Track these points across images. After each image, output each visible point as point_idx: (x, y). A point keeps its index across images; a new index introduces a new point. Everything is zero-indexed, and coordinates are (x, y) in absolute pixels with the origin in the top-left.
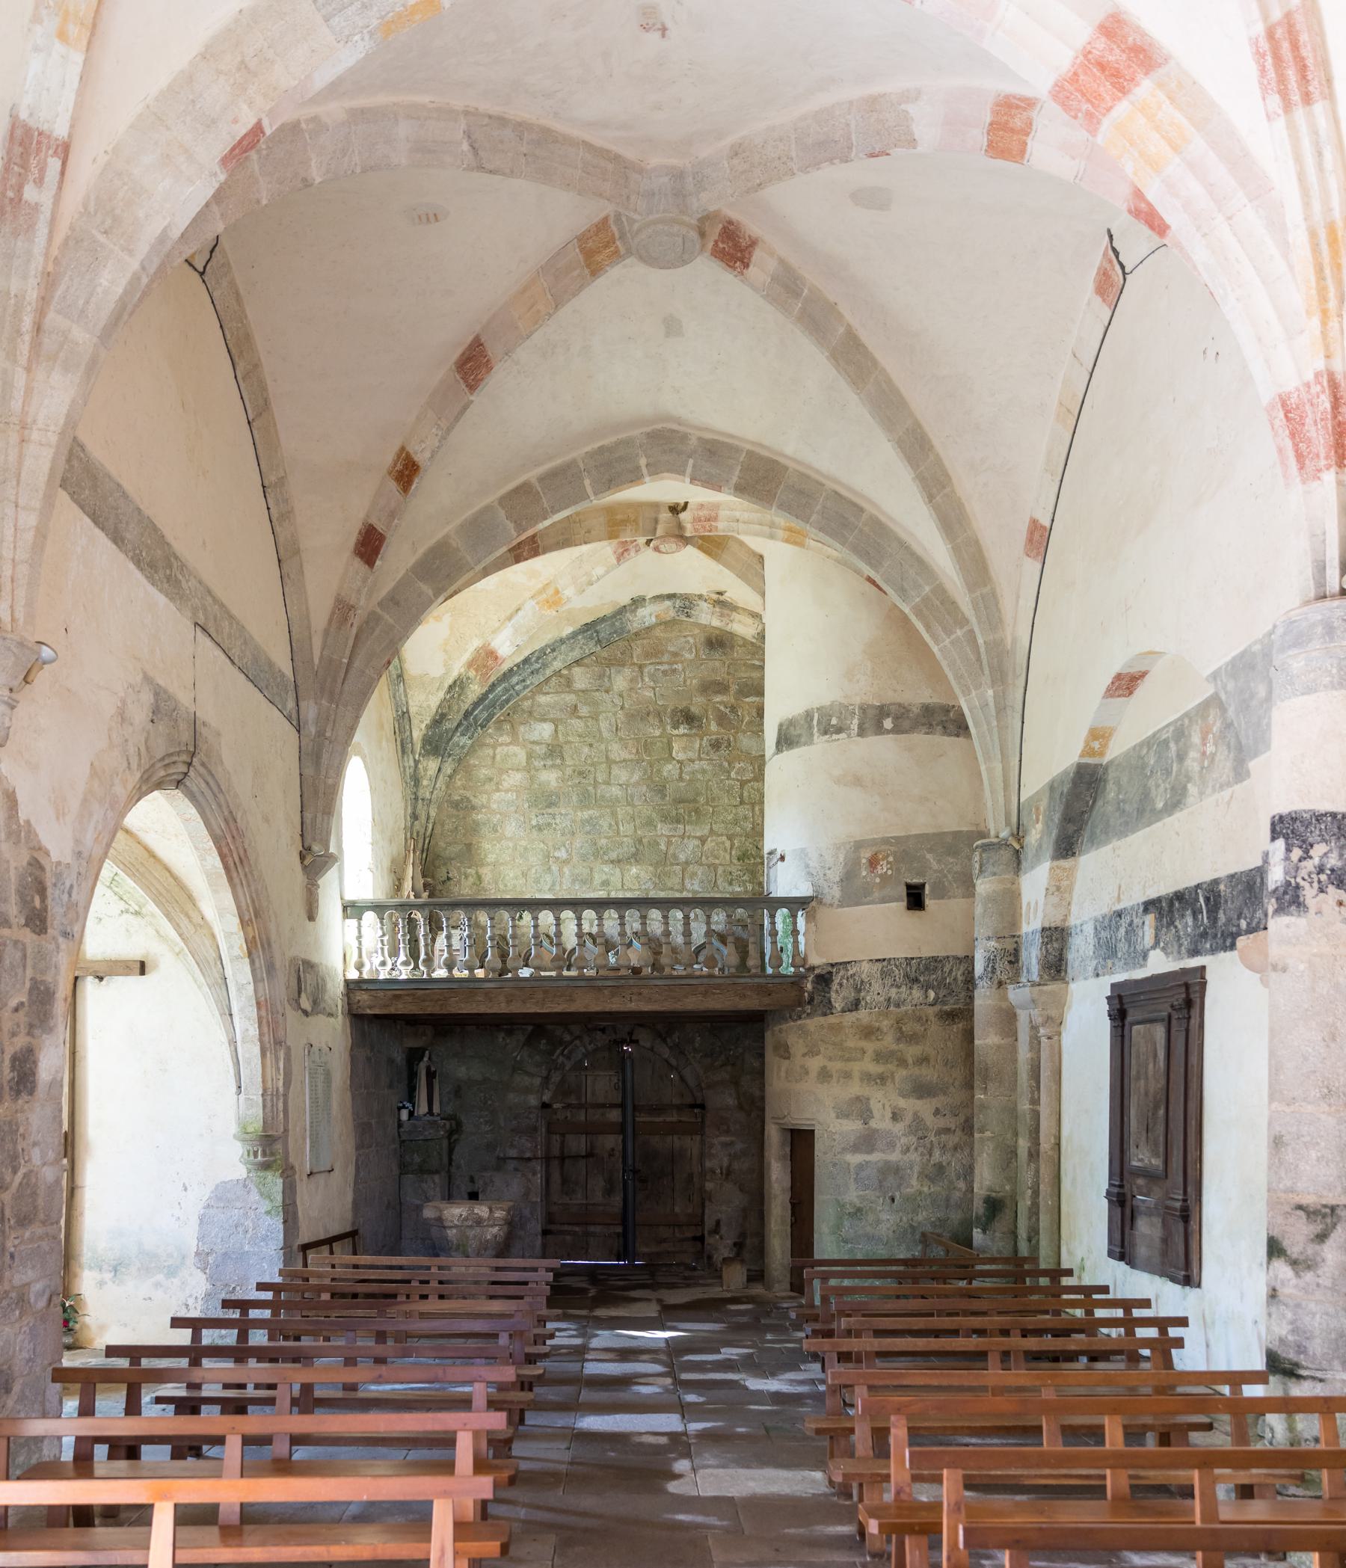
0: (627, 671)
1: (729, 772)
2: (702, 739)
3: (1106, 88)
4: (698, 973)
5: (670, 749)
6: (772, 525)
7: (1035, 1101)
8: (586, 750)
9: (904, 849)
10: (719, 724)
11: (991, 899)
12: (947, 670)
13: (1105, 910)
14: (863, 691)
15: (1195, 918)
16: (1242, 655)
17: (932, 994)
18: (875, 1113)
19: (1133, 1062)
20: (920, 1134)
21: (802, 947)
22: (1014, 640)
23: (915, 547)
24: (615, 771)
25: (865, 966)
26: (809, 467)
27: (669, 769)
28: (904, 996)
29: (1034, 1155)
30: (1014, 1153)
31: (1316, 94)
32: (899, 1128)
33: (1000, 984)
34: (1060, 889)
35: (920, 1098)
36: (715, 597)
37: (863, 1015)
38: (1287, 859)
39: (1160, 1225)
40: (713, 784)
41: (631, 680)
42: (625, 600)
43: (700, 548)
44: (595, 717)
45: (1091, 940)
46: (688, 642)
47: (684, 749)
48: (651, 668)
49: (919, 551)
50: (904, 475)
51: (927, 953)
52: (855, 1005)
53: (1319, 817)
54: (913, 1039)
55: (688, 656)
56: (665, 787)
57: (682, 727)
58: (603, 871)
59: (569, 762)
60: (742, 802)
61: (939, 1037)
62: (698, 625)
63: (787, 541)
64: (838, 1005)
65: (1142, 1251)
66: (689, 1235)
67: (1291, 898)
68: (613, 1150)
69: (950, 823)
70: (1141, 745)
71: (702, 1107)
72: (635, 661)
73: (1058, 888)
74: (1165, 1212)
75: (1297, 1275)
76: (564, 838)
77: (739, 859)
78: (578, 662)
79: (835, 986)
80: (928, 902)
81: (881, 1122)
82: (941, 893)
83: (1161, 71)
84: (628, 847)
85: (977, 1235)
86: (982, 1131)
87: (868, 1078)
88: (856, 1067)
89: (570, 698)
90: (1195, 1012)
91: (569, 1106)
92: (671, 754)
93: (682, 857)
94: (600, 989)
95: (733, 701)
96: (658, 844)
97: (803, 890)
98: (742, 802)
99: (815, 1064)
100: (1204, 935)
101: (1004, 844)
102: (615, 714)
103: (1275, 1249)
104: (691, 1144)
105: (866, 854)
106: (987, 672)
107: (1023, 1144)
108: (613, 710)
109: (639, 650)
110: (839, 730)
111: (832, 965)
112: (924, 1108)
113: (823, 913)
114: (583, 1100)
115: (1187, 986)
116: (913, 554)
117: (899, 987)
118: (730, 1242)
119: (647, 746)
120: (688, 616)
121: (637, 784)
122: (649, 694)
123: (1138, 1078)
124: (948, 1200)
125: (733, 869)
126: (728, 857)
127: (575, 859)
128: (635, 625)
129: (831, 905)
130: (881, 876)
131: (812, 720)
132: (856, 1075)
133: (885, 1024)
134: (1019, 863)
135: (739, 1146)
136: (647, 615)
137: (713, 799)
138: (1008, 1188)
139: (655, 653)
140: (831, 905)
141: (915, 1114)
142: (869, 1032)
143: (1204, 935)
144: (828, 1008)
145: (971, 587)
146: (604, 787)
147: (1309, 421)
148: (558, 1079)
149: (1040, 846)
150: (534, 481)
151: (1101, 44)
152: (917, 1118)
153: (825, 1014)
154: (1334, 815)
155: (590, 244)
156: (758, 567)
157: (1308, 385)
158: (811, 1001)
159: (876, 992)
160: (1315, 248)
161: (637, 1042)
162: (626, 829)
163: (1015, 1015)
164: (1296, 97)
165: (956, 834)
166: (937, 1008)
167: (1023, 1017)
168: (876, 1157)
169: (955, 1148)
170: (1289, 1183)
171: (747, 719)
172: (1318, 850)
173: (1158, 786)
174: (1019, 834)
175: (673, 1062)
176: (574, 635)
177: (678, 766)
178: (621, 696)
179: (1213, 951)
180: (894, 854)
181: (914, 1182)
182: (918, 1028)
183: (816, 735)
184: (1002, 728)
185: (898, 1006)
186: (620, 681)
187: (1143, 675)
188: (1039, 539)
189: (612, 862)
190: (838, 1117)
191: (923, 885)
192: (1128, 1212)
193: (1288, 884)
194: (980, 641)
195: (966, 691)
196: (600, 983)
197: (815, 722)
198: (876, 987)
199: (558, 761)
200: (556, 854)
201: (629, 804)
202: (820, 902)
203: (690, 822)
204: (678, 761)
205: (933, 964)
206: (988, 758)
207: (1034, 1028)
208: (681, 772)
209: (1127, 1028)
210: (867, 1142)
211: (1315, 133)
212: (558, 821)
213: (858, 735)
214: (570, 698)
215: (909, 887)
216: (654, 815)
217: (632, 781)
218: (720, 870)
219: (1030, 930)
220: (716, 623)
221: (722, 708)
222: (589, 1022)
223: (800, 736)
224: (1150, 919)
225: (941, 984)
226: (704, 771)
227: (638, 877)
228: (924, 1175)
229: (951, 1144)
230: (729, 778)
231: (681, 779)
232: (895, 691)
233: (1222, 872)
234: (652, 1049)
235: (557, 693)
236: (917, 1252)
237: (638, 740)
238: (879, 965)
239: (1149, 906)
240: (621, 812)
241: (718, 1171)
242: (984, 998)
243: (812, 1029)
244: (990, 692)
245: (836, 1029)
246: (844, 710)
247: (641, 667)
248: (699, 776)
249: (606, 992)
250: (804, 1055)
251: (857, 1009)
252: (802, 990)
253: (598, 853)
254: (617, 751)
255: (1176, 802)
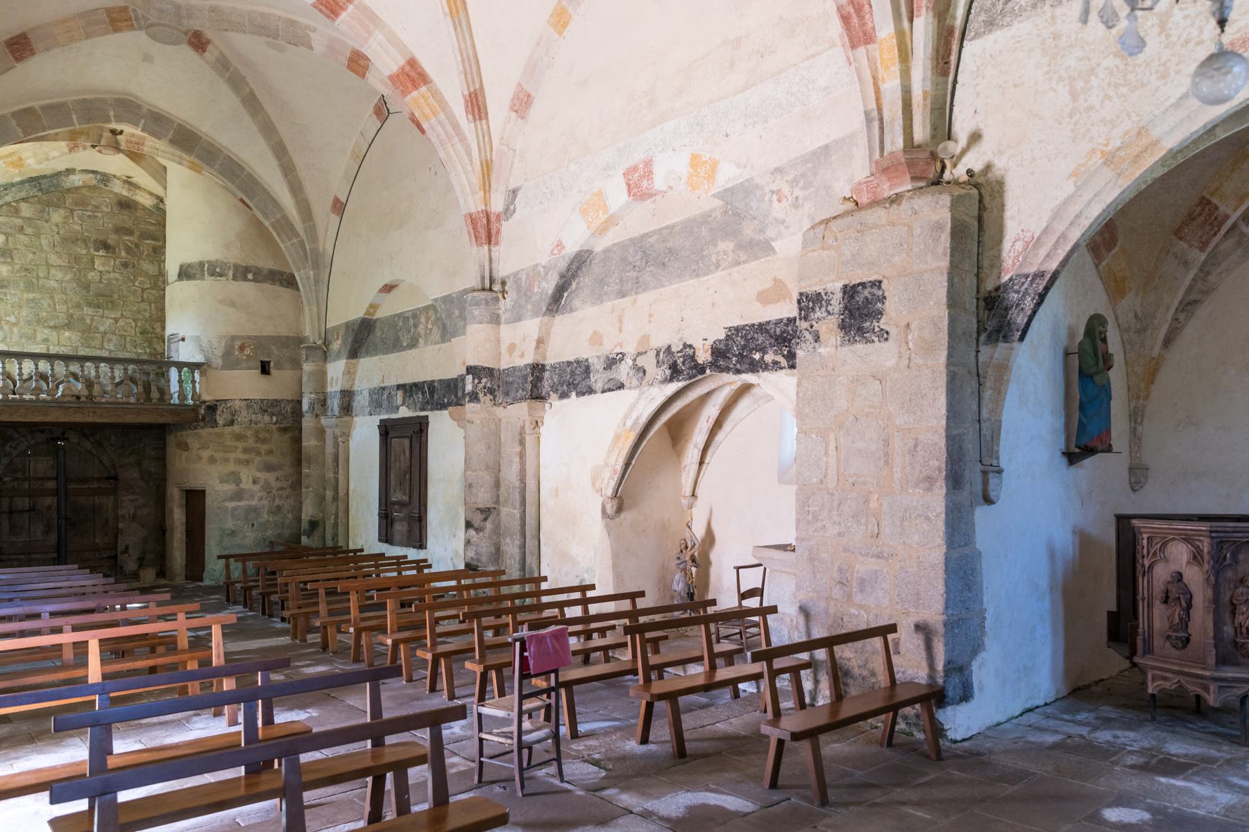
0: (62, 211)
1: (134, 282)
2: (115, 260)
3: (409, 84)
4: (120, 400)
5: (93, 263)
6: (181, 158)
7: (336, 473)
8: (31, 256)
9: (260, 343)
10: (127, 253)
11: (310, 374)
12: (288, 257)
13: (375, 386)
14: (235, 256)
15: (423, 395)
16: (449, 296)
17: (275, 419)
18: (243, 480)
19: (393, 454)
20: (268, 490)
21: (198, 390)
22: (324, 250)
23: (272, 193)
24: (53, 271)
25: (237, 403)
26: (215, 141)
27: (92, 275)
28: (259, 419)
29: (335, 498)
30: (323, 498)
31: (483, 118)
32: (256, 488)
33: (317, 415)
34: (350, 373)
35: (268, 471)
36: (125, 178)
37: (236, 428)
38: (473, 382)
39: (406, 525)
40: (123, 287)
41: (65, 218)
42: (62, 168)
43: (127, 156)
44: (38, 235)
45: (367, 398)
46: (105, 201)
47: (103, 264)
48: (80, 212)
49: (275, 197)
50: (272, 162)
51: (272, 397)
52: (232, 423)
53: (484, 369)
54: (264, 441)
55: (105, 209)
56: (89, 286)
57: (101, 251)
58: (43, 333)
59: (17, 261)
60: (143, 301)
61: (280, 442)
62: (111, 192)
63: (190, 168)
64: (221, 421)
65: (397, 537)
66: (105, 555)
67: (474, 397)
68: (50, 506)
69: (284, 332)
70: (395, 316)
71: (116, 478)
72: (67, 206)
73: (349, 372)
74: (410, 519)
75: (477, 533)
76: (13, 309)
77: (141, 334)
78: (23, 200)
79: (219, 412)
80: (272, 371)
81: (246, 484)
82: (279, 367)
83: (430, 85)
84: (62, 318)
85: (304, 540)
86: (307, 487)
87: (239, 462)
88: (232, 456)
89: (18, 222)
90: (424, 434)
91: (17, 479)
92: (94, 266)
93: (102, 329)
94: (66, 408)
95: (136, 241)
96: (84, 319)
97: (198, 358)
98: (143, 301)
99: (206, 454)
100: (428, 403)
101: (319, 348)
102: (53, 236)
103: (469, 525)
104: (108, 502)
105: (237, 344)
106: (310, 262)
107: (329, 494)
108: (52, 234)
109: (70, 200)
110: (221, 275)
111: (217, 401)
112: (270, 477)
113: (211, 373)
114: (27, 475)
115: (420, 423)
116: (271, 197)
117: (257, 414)
118: (135, 558)
119: (77, 259)
120: (105, 185)
121: (68, 281)
122: (78, 228)
123: (395, 462)
124: (283, 524)
125: (137, 339)
126: (133, 332)
127: (22, 323)
128: (68, 184)
129: (217, 368)
130: (246, 355)
131: (204, 267)
132: (232, 460)
133: (249, 433)
134: (326, 357)
135: (141, 501)
136: (76, 180)
137: (124, 297)
138: (321, 515)
139: (82, 203)
140: (217, 368)
141: (266, 480)
142: (239, 437)
143: (428, 403)
144: (214, 424)
145: (304, 221)
146: (44, 280)
147: (479, 225)
148: (6, 462)
149: (339, 352)
150: (37, 107)
151: (408, 68)
152: (267, 483)
153: (213, 427)
154: (489, 368)
155: (114, 15)
156: (163, 173)
157: (478, 212)
158: (203, 419)
159: (243, 417)
160: (482, 167)
161: (67, 439)
162: (61, 308)
163: (324, 431)
164: (477, 117)
165: (287, 337)
166: (277, 426)
167: (329, 432)
168: (243, 503)
169: (287, 497)
170: (474, 500)
171: (146, 252)
172: (484, 380)
173: (403, 336)
174: (326, 343)
175: (94, 452)
176: (22, 183)
177: (99, 274)
178: (57, 225)
179: (432, 410)
180: (254, 344)
181: (265, 516)
182: (267, 435)
183: (206, 276)
184: (317, 291)
185: (256, 424)
186: (57, 216)
187: (396, 286)
188: (339, 207)
189: (51, 327)
190: (220, 483)
191: (269, 362)
192: (389, 520)
193: (473, 391)
194: (307, 248)
195: (299, 270)
196: (67, 405)
197: (206, 269)
198: (244, 413)
199: (9, 260)
200: (7, 319)
201: (63, 293)
202: (209, 366)
203: (107, 309)
204: (99, 271)
205: (276, 403)
206: (309, 304)
207: (336, 438)
208: (101, 278)
209: (389, 440)
210: (239, 495)
211: (482, 129)
212: (8, 298)
213: (233, 280)
214: (18, 222)
215: (262, 362)
216: (82, 302)
217: (65, 279)
218: (128, 339)
219: (333, 390)
220: (125, 193)
221: (129, 244)
222: (33, 427)
223: (195, 274)
224: (400, 393)
225: (280, 413)
226: (117, 280)
227: (70, 338)
228: (270, 512)
229: (284, 495)
230: (134, 285)
231: (101, 282)
232: (254, 260)
233: (436, 378)
234: (79, 444)
235: (7, 216)
236: (268, 550)
237: (70, 255)
238: (245, 402)
239: (399, 387)
240: (57, 298)
241: (127, 516)
242: (307, 422)
243: (204, 435)
244: (312, 273)
245: (220, 435)
246: (224, 265)
247: (72, 211)
248: (114, 282)
249: (71, 410)
250: (199, 449)
251: (232, 425)
252: (198, 413)
253: (39, 321)
254: (53, 259)
255: (413, 344)
